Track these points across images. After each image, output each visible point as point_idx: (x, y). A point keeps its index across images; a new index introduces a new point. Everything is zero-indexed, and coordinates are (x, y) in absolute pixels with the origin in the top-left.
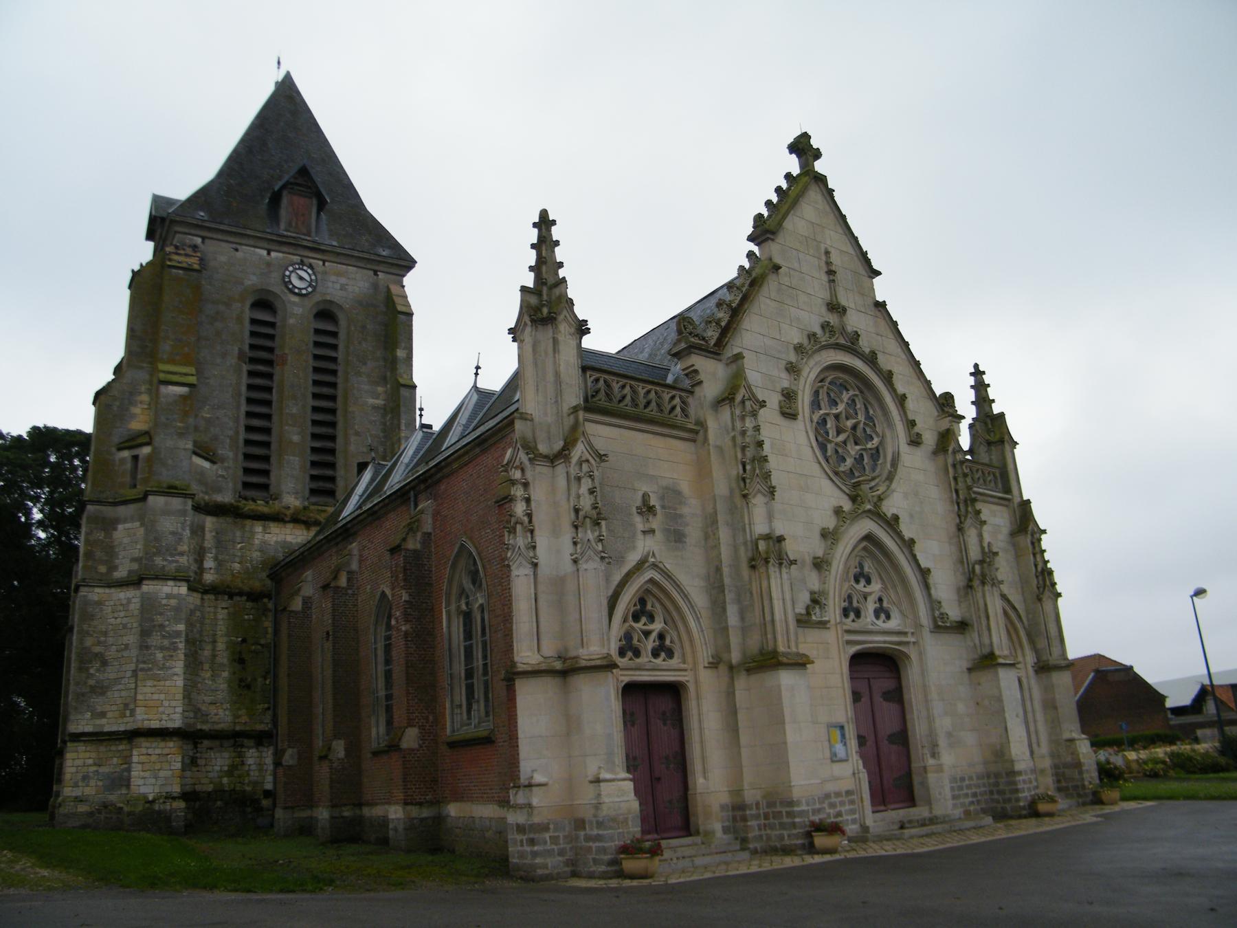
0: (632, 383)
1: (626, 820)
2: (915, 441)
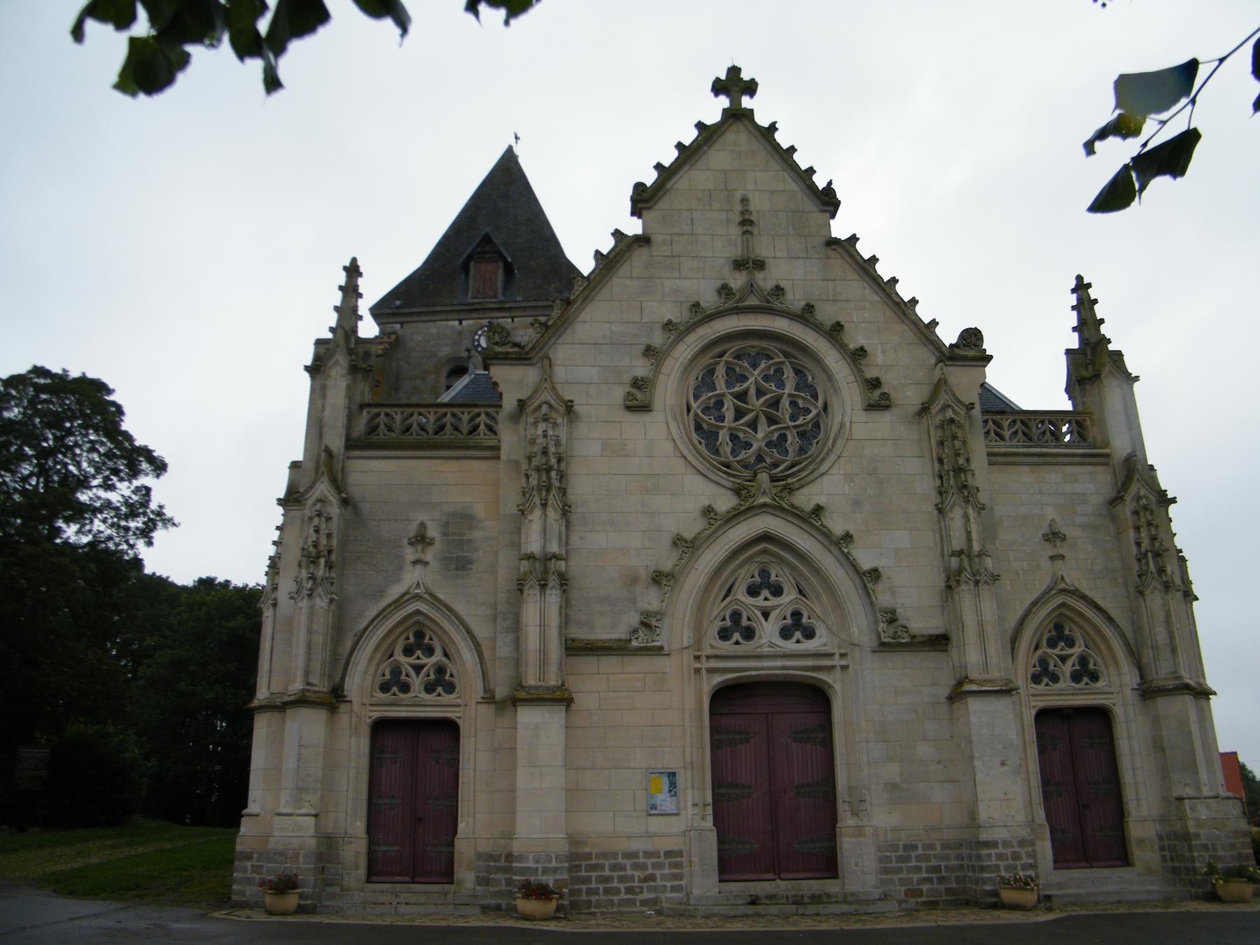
0: (388, 410)
1: (297, 855)
2: (879, 402)
